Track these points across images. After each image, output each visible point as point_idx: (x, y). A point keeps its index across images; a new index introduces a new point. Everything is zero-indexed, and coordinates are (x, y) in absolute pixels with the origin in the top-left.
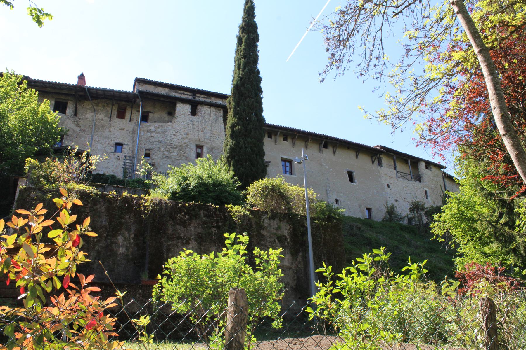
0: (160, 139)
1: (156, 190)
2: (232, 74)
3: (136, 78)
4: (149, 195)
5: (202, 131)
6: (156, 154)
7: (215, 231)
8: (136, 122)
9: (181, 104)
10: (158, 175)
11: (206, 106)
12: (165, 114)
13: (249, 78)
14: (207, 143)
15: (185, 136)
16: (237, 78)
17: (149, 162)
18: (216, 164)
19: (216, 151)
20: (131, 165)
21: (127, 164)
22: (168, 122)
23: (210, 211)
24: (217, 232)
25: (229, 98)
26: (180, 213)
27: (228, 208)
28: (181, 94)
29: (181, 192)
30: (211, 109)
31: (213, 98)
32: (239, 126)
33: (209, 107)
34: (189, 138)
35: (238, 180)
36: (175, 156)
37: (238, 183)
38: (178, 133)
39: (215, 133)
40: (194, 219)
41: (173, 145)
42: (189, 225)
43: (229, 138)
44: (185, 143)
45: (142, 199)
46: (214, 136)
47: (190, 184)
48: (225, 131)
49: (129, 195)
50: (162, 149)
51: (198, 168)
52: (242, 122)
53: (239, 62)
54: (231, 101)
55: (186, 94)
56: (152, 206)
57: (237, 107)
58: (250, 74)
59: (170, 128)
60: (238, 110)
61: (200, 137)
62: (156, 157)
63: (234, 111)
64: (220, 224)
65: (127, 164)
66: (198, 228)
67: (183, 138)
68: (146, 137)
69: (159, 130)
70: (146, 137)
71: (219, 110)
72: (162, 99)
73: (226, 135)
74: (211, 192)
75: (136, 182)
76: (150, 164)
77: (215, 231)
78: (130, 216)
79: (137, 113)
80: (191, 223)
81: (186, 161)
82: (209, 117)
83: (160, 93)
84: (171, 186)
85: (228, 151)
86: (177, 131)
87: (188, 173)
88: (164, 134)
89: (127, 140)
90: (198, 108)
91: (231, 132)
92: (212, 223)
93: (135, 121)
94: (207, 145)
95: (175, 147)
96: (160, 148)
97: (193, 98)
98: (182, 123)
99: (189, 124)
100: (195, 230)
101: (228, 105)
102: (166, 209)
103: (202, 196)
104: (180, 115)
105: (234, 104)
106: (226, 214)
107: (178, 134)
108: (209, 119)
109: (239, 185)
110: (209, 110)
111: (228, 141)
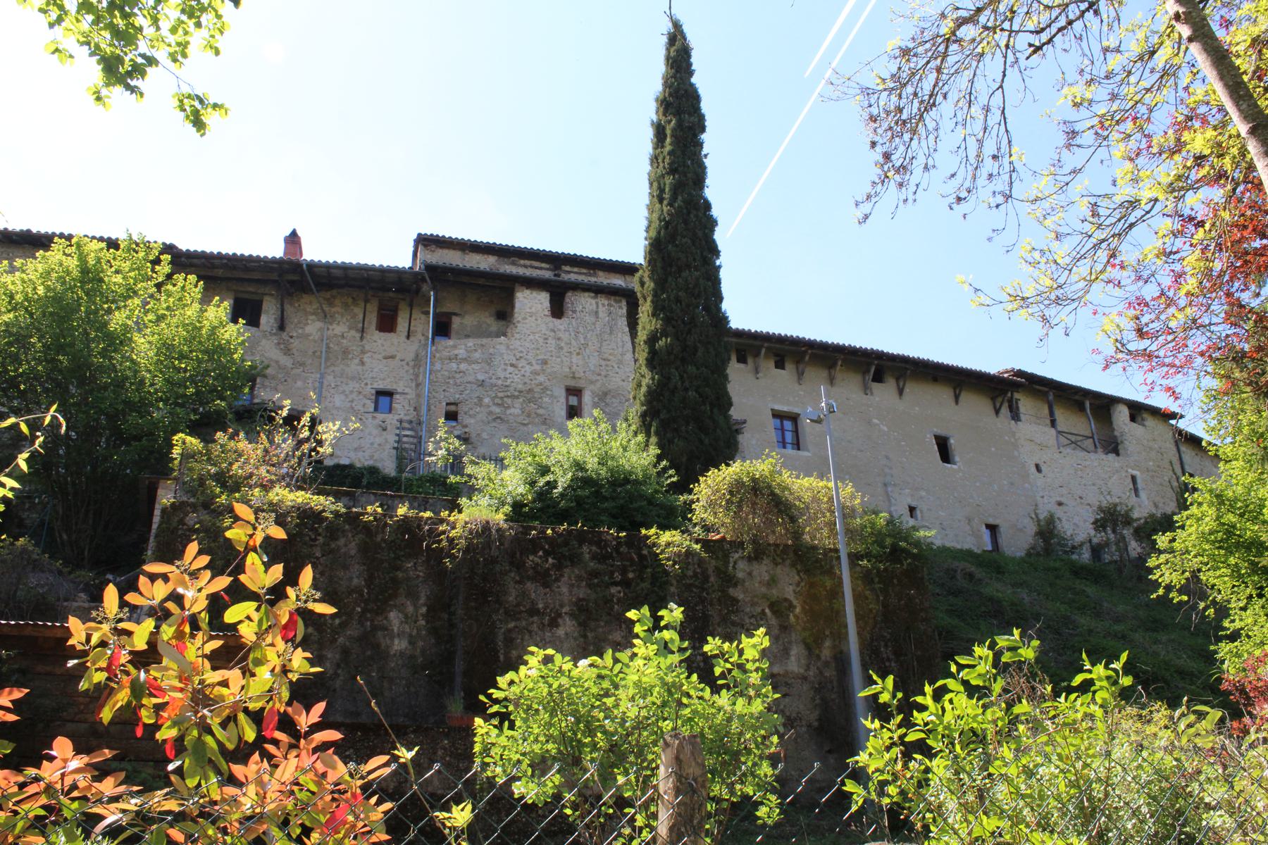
0: (481, 377)
1: (475, 498)
2: (646, 213)
3: (419, 235)
4: (460, 512)
5: (578, 354)
6: (471, 412)
7: (620, 592)
8: (422, 338)
9: (527, 292)
10: (478, 463)
11: (586, 294)
12: (490, 316)
13: (686, 222)
14: (592, 382)
15: (538, 367)
16: (656, 224)
17: (456, 433)
18: (614, 430)
19: (614, 400)
20: (415, 441)
21: (405, 439)
22: (498, 336)
23: (606, 545)
24: (625, 594)
25: (641, 272)
26: (535, 553)
27: (648, 537)
28: (526, 267)
29: (534, 501)
30: (599, 300)
31: (601, 273)
32: (666, 338)
33: (593, 295)
34: (549, 371)
35: (671, 468)
36: (518, 416)
37: (671, 476)
38: (522, 360)
39: (611, 357)
40: (567, 567)
41: (512, 389)
42: (557, 580)
43: (644, 368)
44: (541, 384)
45: (442, 521)
46: (607, 365)
47: (555, 481)
48: (634, 352)
49: (412, 513)
50: (487, 400)
51: (574, 442)
52: (674, 327)
53: (659, 184)
54: (646, 279)
55: (536, 268)
56: (466, 538)
57: (659, 292)
58: (689, 213)
59: (502, 348)
60: (664, 300)
61: (574, 368)
62: (472, 421)
63: (652, 302)
64: (631, 575)
65: (405, 439)
66: (579, 587)
67: (535, 373)
68: (446, 373)
69: (477, 355)
70: (446, 373)
71: (616, 301)
72: (481, 281)
73: (636, 361)
74: (605, 499)
75: (428, 481)
76: (458, 437)
77: (620, 592)
78: (415, 564)
79: (423, 317)
80: (562, 576)
81: (544, 427)
82: (593, 319)
83: (475, 266)
84: (510, 488)
85: (643, 398)
86: (518, 355)
87: (549, 457)
88: (489, 364)
89: (401, 384)
90: (567, 300)
91: (649, 353)
92: (612, 573)
93: (420, 336)
94: (592, 387)
95: (516, 393)
96: (480, 399)
97: (555, 275)
98: (531, 337)
99: (546, 339)
100: (570, 592)
101: (637, 288)
102: (501, 544)
103: (585, 510)
104: (525, 319)
105: (652, 285)
106: (645, 552)
107: (522, 363)
108: (594, 324)
109: (674, 479)
110: (593, 302)
111: (643, 376)
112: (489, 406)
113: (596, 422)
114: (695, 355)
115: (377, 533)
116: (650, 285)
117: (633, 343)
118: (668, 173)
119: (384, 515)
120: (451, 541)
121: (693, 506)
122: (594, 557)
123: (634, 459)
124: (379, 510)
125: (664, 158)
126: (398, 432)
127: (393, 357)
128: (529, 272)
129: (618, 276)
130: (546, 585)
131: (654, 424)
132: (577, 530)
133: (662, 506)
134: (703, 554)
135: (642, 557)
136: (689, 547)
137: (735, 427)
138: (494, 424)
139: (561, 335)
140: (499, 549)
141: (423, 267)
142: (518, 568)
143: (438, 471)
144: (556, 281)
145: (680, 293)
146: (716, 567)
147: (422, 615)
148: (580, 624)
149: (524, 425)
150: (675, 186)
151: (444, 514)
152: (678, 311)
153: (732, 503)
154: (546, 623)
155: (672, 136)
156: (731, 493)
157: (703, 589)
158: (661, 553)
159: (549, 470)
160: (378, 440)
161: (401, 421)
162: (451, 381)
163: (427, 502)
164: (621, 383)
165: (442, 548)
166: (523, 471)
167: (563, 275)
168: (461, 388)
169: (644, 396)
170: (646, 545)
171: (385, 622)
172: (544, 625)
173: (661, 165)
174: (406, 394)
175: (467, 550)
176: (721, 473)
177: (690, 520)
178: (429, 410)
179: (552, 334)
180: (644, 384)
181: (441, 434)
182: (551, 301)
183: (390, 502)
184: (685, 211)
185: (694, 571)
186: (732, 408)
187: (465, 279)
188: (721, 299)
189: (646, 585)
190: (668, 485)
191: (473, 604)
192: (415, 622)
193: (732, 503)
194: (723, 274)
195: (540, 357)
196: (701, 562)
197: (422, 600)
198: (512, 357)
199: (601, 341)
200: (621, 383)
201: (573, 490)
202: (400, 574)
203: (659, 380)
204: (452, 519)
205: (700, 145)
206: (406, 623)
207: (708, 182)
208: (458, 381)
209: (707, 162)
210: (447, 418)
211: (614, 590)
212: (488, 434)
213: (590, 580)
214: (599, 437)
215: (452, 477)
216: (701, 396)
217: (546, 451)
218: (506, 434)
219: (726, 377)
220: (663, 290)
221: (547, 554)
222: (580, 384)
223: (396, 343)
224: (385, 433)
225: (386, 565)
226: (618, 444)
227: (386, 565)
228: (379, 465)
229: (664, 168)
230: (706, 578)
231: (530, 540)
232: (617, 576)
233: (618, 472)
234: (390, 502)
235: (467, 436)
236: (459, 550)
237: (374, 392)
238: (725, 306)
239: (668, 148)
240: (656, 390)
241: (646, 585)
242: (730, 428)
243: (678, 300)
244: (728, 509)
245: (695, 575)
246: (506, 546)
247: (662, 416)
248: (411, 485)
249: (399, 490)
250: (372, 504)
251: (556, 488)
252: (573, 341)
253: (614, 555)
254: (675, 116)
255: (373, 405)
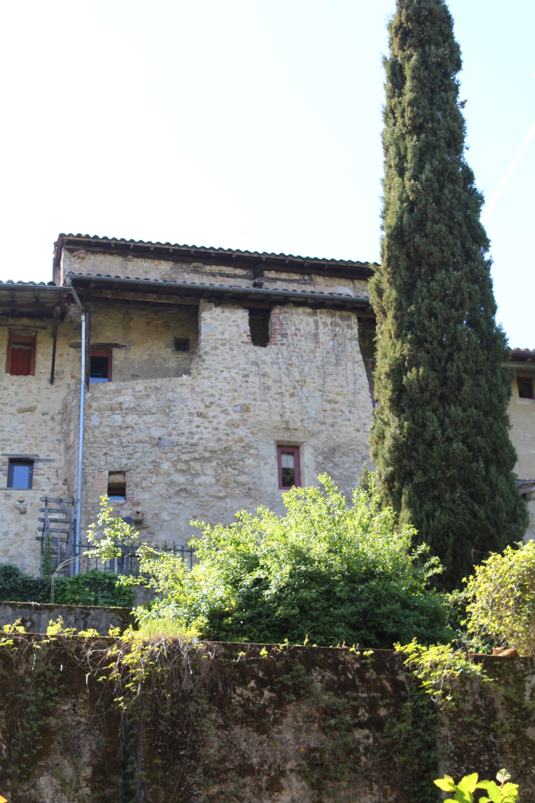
0: (156, 433)
1: (155, 607)
2: (380, 191)
3: (62, 236)
4: (136, 627)
5: (292, 395)
6: (145, 484)
7: (367, 737)
8: (72, 382)
9: (217, 311)
10: (157, 557)
11: (300, 310)
12: (167, 347)
13: (438, 202)
14: (313, 435)
15: (236, 417)
16: (396, 206)
17: (125, 513)
18: (349, 502)
19: (345, 458)
20: (67, 527)
21: (52, 525)
22: (178, 375)
23: (346, 669)
24: (376, 740)
25: (377, 275)
27: (405, 656)
28: (213, 275)
29: (240, 608)
30: (318, 318)
31: (319, 279)
32: (418, 368)
33: (309, 310)
34: (251, 420)
36: (211, 486)
37: (433, 566)
38: (214, 407)
39: (338, 398)
40: (290, 702)
41: (200, 448)
42: (277, 722)
43: (387, 412)
44: (241, 440)
45: (111, 642)
46: (334, 410)
48: (372, 389)
49: (68, 632)
50: (166, 466)
51: (292, 521)
52: (428, 352)
53: (398, 149)
54: (385, 286)
55: (228, 276)
56: (146, 666)
57: (404, 303)
58: (442, 187)
59: (185, 392)
60: (412, 314)
61: (287, 415)
62: (147, 496)
63: (395, 317)
64: (383, 712)
65: (52, 525)
66: (308, 730)
67: (234, 425)
68: (107, 430)
69: (150, 403)
70: (107, 430)
71: (343, 318)
72: (152, 298)
73: (375, 402)
74: (341, 601)
75: (87, 584)
76: (128, 520)
77: (367, 737)
78: (74, 705)
79: (72, 351)
80: (283, 715)
81: (247, 501)
82: (312, 345)
83: (142, 277)
84: (205, 591)
85: (387, 455)
86: (208, 401)
87: (258, 544)
88: (167, 415)
89: (44, 446)
90: (273, 319)
91: (393, 391)
92: (355, 710)
93: (68, 379)
94: (314, 441)
95: (207, 455)
96: (156, 464)
97: (255, 285)
98: (225, 374)
99: (247, 376)
100: (297, 738)
101: (373, 299)
102: (196, 673)
103: (313, 619)
104: (215, 348)
105: (394, 293)
106: (401, 677)
107: (214, 411)
108: (313, 352)
109: (439, 570)
110: (311, 320)
111: (386, 424)
112: (169, 474)
113: (323, 491)
114: (459, 390)
115: (19, 662)
116: (390, 293)
117: (370, 378)
118: (409, 132)
119: (29, 637)
120: (125, 670)
121: (468, 609)
122: (328, 687)
123: (380, 542)
124: (21, 630)
125: (403, 111)
126: (42, 515)
127: (31, 410)
128: (227, 284)
129: (343, 281)
130: (262, 730)
131: (405, 491)
132: (302, 648)
133: (422, 610)
134: (487, 679)
135: (397, 685)
136: (465, 668)
137: (521, 491)
138: (178, 499)
139: (267, 370)
140: (194, 680)
141: (69, 281)
142: (221, 707)
143: (101, 569)
144: (256, 294)
145: (434, 303)
146: (507, 698)
147: (86, 780)
148: (313, 786)
149: (221, 498)
150: (420, 149)
151: (114, 632)
152: (433, 329)
153: (525, 602)
154: (264, 785)
155: (413, 78)
156: (522, 587)
157: (489, 730)
158: (425, 679)
159: (257, 564)
160: (14, 528)
161: (46, 501)
162: (115, 441)
163: (88, 615)
164: (355, 434)
165: (112, 683)
166: (222, 565)
167: (266, 284)
168: (129, 450)
169: (390, 452)
170: (402, 667)
171: (33, 791)
172: (261, 789)
173: (400, 120)
174: (52, 461)
175: (147, 683)
176: (505, 559)
177: (464, 628)
178: (85, 483)
179: (254, 368)
180: (388, 434)
181: (104, 516)
182: (251, 323)
183: (35, 617)
184: (436, 185)
185: (474, 705)
186: (517, 464)
187: (130, 296)
188: (493, 309)
189: (405, 726)
190: (430, 578)
191: (158, 761)
192: (77, 791)
193: (525, 602)
194: (494, 273)
195: (238, 402)
196: (483, 691)
197: (86, 758)
198: (199, 403)
199: (325, 376)
200: (355, 434)
201: (294, 590)
202: (53, 721)
203: (409, 428)
204: (124, 638)
205: (455, 89)
206: (63, 791)
207: (467, 141)
208: (124, 440)
209: (464, 112)
210: (110, 495)
211: (359, 734)
212: (170, 514)
213: (325, 720)
214: (329, 513)
215: (122, 577)
216: (470, 449)
217: (253, 536)
218: (196, 512)
219: (505, 420)
220: (410, 300)
221: (262, 684)
222: (296, 438)
223: (34, 390)
224: (23, 517)
225: (32, 708)
226: (356, 522)
227: (32, 708)
228: (17, 563)
229: (404, 125)
230: (492, 715)
231: (237, 666)
232: (364, 715)
233: (357, 562)
234: (35, 617)
235: (140, 517)
236: (136, 683)
237: (6, 460)
238: (499, 319)
239: (408, 96)
240: (405, 444)
241: (405, 726)
242: (514, 493)
243: (432, 314)
244: (518, 611)
245: (476, 709)
246: (203, 675)
247: (416, 480)
248: (64, 590)
249: (46, 598)
250: (10, 621)
251: (267, 588)
252: (284, 378)
253: (357, 682)
254: (415, 48)
255: (6, 479)
